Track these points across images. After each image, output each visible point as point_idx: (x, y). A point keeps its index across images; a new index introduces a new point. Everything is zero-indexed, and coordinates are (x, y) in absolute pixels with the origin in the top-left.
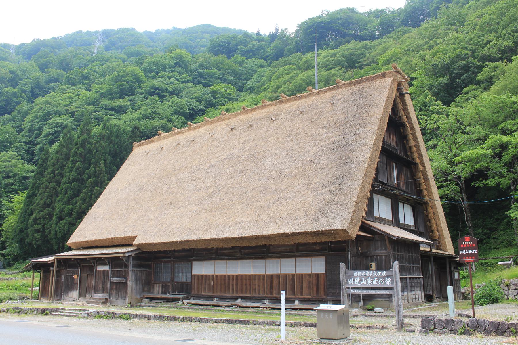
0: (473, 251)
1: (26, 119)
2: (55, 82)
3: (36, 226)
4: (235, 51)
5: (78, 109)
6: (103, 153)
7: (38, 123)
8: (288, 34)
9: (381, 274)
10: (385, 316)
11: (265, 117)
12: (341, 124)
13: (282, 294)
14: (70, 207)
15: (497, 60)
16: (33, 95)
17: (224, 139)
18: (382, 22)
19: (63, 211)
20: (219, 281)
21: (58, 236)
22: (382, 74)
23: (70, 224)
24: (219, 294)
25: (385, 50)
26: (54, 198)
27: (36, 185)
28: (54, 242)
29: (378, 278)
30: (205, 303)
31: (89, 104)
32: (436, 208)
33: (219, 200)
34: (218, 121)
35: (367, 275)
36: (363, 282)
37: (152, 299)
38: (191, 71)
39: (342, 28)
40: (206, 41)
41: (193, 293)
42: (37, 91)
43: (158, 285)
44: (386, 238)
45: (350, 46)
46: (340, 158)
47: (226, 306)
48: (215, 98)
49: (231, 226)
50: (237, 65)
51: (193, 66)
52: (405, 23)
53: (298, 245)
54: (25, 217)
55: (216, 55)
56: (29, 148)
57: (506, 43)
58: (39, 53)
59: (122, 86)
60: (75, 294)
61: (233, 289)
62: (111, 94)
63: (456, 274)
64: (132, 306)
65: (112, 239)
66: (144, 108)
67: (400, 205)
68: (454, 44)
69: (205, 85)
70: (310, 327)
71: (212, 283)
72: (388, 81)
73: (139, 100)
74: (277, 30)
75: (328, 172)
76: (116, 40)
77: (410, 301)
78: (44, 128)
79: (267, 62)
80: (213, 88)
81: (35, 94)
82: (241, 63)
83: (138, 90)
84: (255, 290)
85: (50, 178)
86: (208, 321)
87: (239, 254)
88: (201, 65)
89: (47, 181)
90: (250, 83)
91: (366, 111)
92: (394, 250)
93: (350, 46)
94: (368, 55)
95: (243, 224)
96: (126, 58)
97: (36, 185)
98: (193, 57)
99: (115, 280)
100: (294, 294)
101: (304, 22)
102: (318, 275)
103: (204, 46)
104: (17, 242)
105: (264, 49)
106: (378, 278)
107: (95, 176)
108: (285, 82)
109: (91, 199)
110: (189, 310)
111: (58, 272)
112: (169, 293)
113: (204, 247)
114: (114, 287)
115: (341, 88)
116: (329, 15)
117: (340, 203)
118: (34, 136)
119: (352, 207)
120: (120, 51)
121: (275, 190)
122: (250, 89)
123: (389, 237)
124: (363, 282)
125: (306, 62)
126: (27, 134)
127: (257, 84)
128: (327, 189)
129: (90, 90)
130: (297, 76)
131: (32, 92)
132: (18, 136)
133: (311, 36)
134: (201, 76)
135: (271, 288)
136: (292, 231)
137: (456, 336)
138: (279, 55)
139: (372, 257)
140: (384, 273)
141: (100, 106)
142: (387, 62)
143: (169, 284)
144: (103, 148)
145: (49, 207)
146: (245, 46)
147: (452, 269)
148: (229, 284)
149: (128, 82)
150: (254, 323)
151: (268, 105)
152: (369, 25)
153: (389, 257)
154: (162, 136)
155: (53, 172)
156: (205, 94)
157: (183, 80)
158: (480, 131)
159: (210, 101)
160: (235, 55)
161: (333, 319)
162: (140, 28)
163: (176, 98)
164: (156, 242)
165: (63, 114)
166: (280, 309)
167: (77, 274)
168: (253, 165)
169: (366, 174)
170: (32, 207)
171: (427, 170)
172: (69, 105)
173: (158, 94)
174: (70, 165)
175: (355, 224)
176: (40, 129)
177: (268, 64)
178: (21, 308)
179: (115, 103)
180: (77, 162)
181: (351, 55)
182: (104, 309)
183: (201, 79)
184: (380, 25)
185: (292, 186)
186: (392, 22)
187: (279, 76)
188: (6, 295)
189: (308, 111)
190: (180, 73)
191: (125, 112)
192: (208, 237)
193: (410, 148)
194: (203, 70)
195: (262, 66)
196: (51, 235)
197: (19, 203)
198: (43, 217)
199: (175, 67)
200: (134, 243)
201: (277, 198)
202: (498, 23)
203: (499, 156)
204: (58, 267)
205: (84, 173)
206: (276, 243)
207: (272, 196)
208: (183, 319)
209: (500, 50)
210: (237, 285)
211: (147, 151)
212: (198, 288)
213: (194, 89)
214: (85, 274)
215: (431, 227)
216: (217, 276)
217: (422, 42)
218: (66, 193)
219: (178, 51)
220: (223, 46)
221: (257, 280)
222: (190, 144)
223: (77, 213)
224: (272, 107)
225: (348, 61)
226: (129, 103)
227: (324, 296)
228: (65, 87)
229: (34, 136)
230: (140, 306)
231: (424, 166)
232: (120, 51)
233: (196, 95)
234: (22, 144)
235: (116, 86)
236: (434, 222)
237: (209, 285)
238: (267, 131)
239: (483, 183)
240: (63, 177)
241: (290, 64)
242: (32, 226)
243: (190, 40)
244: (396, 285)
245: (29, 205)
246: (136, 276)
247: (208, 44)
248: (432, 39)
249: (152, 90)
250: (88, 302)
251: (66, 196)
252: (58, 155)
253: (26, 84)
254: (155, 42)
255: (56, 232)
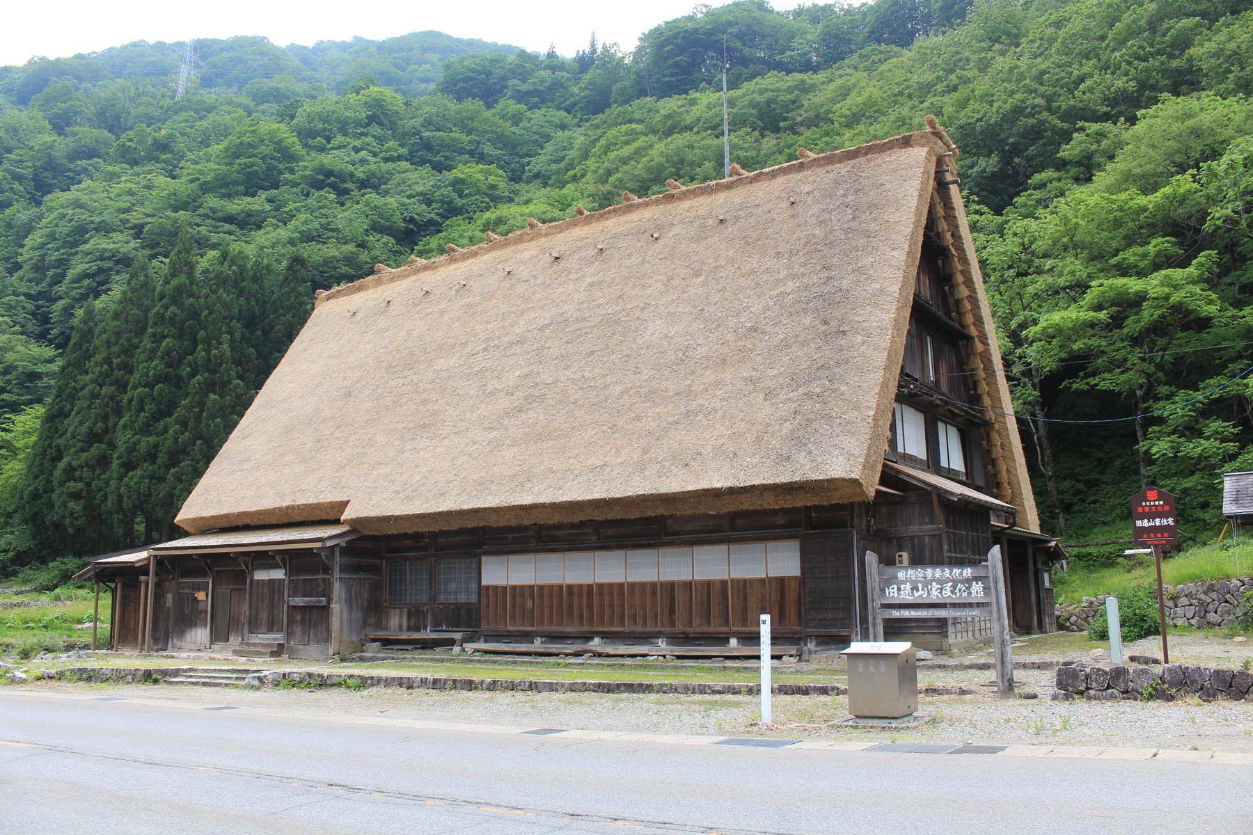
0: (1164, 522)
1: (28, 242)
2: (90, 157)
3: (72, 484)
4: (501, 91)
5: (149, 220)
6: (225, 318)
7: (57, 250)
8: (620, 55)
9: (961, 573)
10: (940, 666)
11: (634, 231)
12: (819, 247)
13: (764, 622)
14: (152, 439)
15: (1105, 118)
16: (39, 188)
17: (539, 282)
18: (828, 33)
19: (134, 450)
20: (546, 598)
21: (125, 505)
22: (904, 138)
23: (151, 477)
24: (547, 628)
25: (844, 94)
26: (112, 420)
27: (67, 391)
28: (116, 520)
29: (955, 583)
30: (517, 650)
31: (176, 210)
32: (1008, 435)
33: (542, 417)
34: (520, 240)
35: (929, 577)
36: (921, 592)
37: (386, 643)
38: (404, 135)
39: (738, 45)
40: (434, 67)
41: (484, 627)
42: (46, 178)
43: (397, 611)
44: (935, 498)
45: (767, 82)
46: (825, 323)
47: (567, 655)
48: (461, 196)
49: (580, 475)
50: (508, 123)
51: (409, 124)
52: (876, 36)
53: (734, 516)
54: (42, 464)
55: (460, 99)
56: (38, 307)
57: (1120, 83)
58: (46, 89)
59: (250, 167)
60: (201, 634)
61: (581, 617)
62: (225, 185)
63: (1046, 576)
64: (343, 660)
65: (287, 508)
66: (303, 217)
67: (941, 427)
68: (1010, 81)
69: (438, 168)
70: (793, 693)
71: (529, 604)
72: (919, 154)
73: (290, 197)
74: (593, 45)
75: (800, 353)
76: (231, 65)
77: (977, 633)
78: (73, 262)
79: (575, 116)
80: (456, 173)
81: (43, 186)
82: (516, 119)
83: (287, 175)
84: (633, 617)
85: (101, 374)
86: (552, 687)
87: (595, 538)
88: (428, 123)
89: (93, 381)
90: (539, 163)
91: (874, 219)
92: (948, 525)
93: (767, 82)
94: (806, 103)
95: (608, 469)
96: (252, 105)
97: (67, 391)
98: (407, 104)
99: (299, 601)
100: (727, 624)
101: (656, 30)
102: (781, 581)
103: (426, 81)
104: (26, 521)
105: (566, 89)
106: (955, 583)
107: (209, 370)
108: (625, 161)
109: (200, 422)
110: (478, 665)
111: (158, 585)
112: (425, 628)
113: (514, 523)
114: (299, 617)
115: (809, 168)
116: (711, 14)
117: (838, 421)
118: (48, 279)
119: (866, 431)
120: (235, 88)
121: (678, 394)
122: (537, 176)
123: (941, 493)
124: (921, 592)
125: (669, 117)
126: (31, 276)
127: (554, 167)
128: (801, 390)
129: (174, 177)
130: (651, 146)
131: (36, 179)
132: (9, 280)
133: (671, 62)
134: (427, 146)
135: (672, 611)
136: (729, 484)
137: (1139, 704)
138: (597, 103)
139: (899, 539)
140: (968, 572)
141: (201, 211)
142: (853, 120)
143: (425, 608)
144: (226, 306)
145: (100, 441)
146: (524, 81)
147: (1040, 566)
148: (571, 605)
149: (263, 158)
150: (663, 689)
151: (638, 206)
152: (798, 40)
153: (941, 540)
154: (385, 276)
155: (108, 361)
156: (439, 188)
157: (387, 155)
158: (1073, 266)
159: (451, 202)
160: (502, 102)
161: (889, 674)
162: (281, 39)
163: (374, 195)
164: (398, 513)
165: (115, 231)
166: (758, 657)
167: (206, 589)
168: (618, 337)
169: (889, 358)
170: (61, 441)
171: (992, 352)
172: (127, 211)
173: (334, 187)
174: (147, 343)
175: (873, 468)
176: (63, 263)
177: (576, 121)
178: (93, 670)
179: (237, 206)
180: (164, 337)
181: (768, 103)
182: (271, 668)
183: (426, 153)
184: (823, 40)
185: (718, 384)
186: (849, 33)
187: (608, 147)
188: (35, 640)
189: (737, 219)
190: (380, 140)
191: (260, 227)
192: (527, 500)
193: (958, 302)
194: (431, 134)
195: (563, 127)
196: (109, 503)
197: (27, 433)
198: (87, 464)
199: (368, 125)
200: (343, 518)
201: (684, 410)
202: (1103, 38)
203: (1117, 322)
204: (157, 574)
205: (180, 362)
206: (689, 512)
207: (671, 406)
208: (493, 686)
209: (1106, 99)
210: (590, 606)
211: (353, 309)
212: (496, 616)
213: (413, 176)
214: (225, 589)
215: (996, 475)
216: (541, 588)
217: (929, 77)
218: (142, 409)
219: (374, 90)
220: (473, 79)
221: (637, 595)
222: (457, 292)
223: (169, 452)
224: (649, 209)
225: (761, 117)
226: (267, 207)
227: (797, 628)
228: (117, 169)
229: (48, 279)
230: (362, 659)
231: (985, 344)
232: (235, 88)
233: (419, 189)
234: (22, 298)
235: (236, 167)
236: (1002, 466)
237: (523, 607)
238: (642, 263)
239: (1087, 384)
240: (131, 372)
241: (630, 122)
242: (62, 484)
243: (396, 66)
244: (997, 597)
245: (51, 438)
246: (349, 591)
247: (440, 75)
248: (952, 71)
249: (321, 177)
250: (236, 652)
251: (143, 414)
252: (117, 323)
253: (21, 161)
254: (316, 71)
255: (120, 496)
